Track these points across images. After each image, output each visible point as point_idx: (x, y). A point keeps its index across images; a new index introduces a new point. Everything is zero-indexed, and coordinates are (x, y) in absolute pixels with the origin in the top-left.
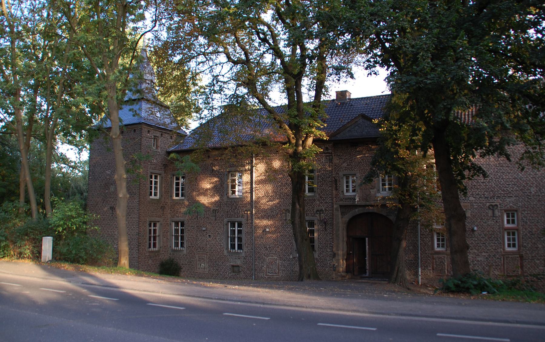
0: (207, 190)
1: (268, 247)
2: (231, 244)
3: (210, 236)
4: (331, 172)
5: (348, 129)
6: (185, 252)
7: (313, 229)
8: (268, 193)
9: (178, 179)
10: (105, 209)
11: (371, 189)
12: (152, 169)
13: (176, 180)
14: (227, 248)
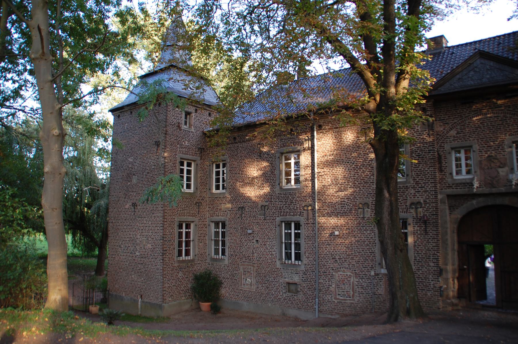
0: (253, 178)
1: (337, 257)
3: (257, 241)
4: (432, 144)
5: (458, 76)
6: (226, 262)
7: (406, 231)
8: (336, 179)
9: (218, 167)
10: (127, 206)
11: (500, 167)
12: (183, 153)
14: (281, 259)
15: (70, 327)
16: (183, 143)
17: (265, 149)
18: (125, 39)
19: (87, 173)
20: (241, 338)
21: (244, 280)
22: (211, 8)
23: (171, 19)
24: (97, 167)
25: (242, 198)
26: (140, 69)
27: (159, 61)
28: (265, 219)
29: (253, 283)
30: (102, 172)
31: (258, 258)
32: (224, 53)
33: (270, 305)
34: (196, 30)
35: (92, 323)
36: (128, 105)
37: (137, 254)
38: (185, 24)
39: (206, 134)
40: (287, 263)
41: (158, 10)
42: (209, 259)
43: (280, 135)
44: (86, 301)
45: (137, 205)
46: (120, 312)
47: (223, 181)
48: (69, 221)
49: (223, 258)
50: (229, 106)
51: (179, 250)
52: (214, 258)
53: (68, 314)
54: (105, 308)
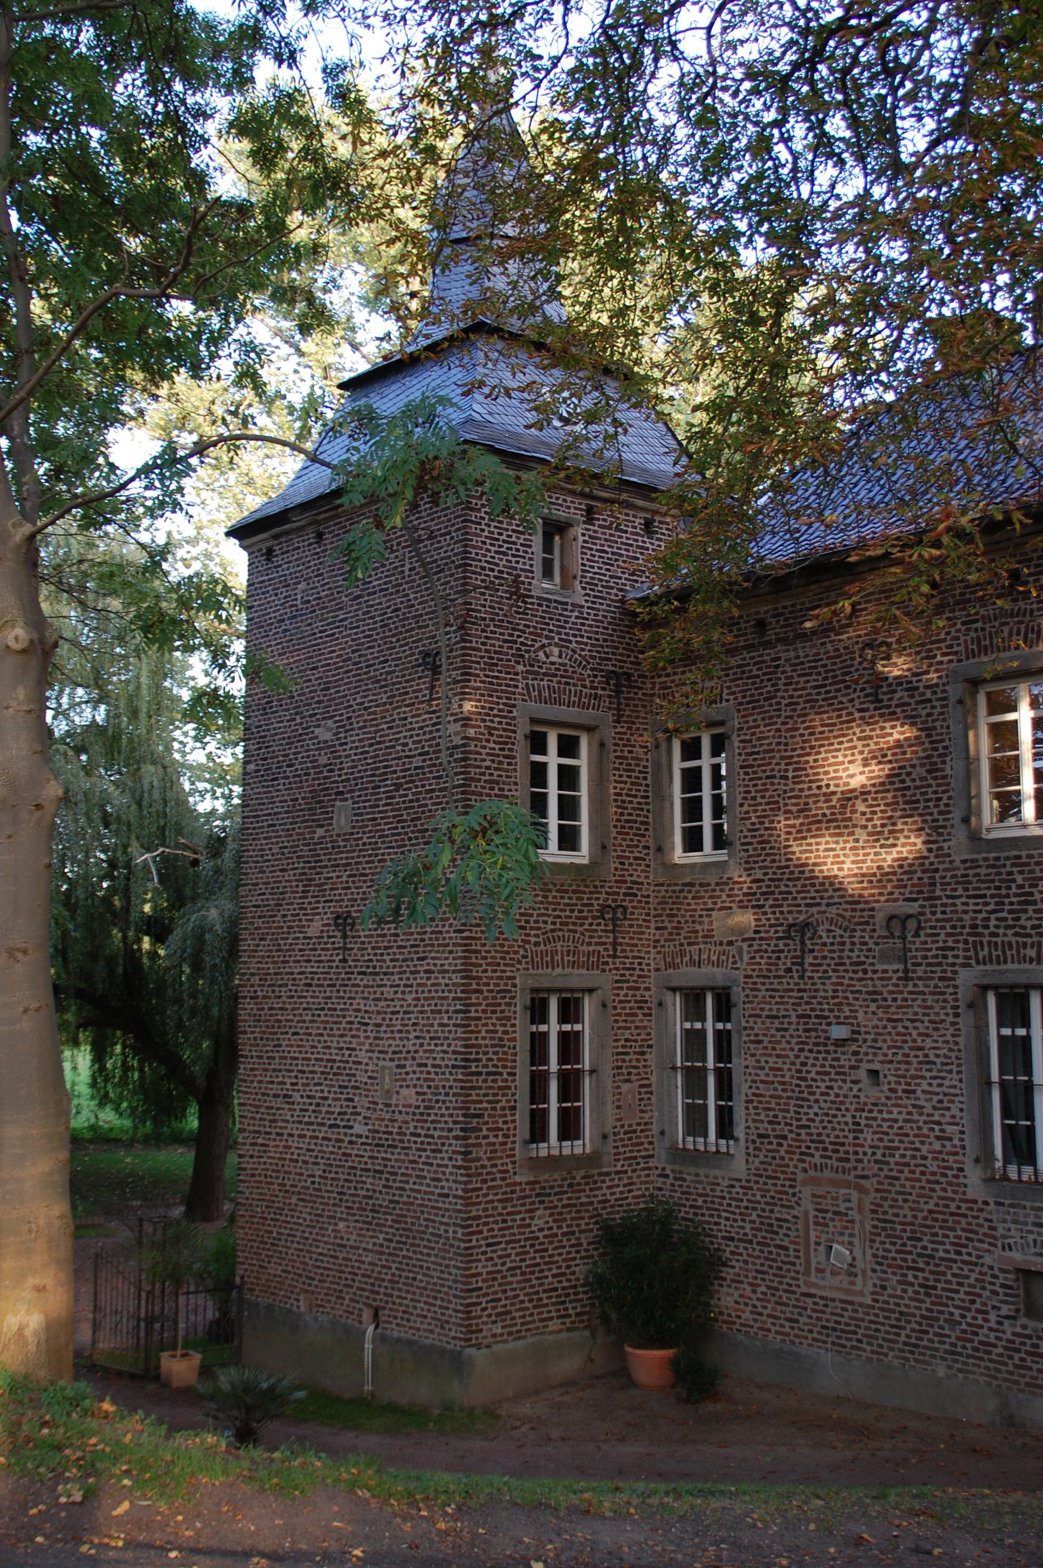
0: (849, 797)
2: (1004, 1127)
3: (874, 1073)
6: (739, 1167)
9: (692, 750)
10: (314, 929)
12: (540, 698)
13: (684, 759)
14: (985, 1157)
15: (79, 1454)
16: (541, 654)
17: (898, 667)
18: (278, 229)
19: (150, 794)
20: (812, 1527)
21: (822, 1249)
22: (632, 57)
23: (464, 126)
24: (190, 767)
25: (799, 883)
26: (346, 348)
27: (424, 313)
28: (906, 978)
29: (859, 1263)
30: (208, 786)
31: (879, 1153)
32: (698, 258)
33: (941, 1372)
34: (575, 167)
35: (169, 1436)
36: (304, 507)
37: (359, 1129)
38: (527, 138)
39: (635, 615)
40: (1014, 1176)
41: (408, 92)
42: (664, 1155)
43: (963, 602)
44: (149, 1332)
45: (353, 925)
46: (285, 1383)
47: (718, 810)
48: (80, 994)
49: (724, 1150)
50: (730, 485)
51: (532, 1110)
52: (684, 1149)
53: (70, 1393)
54: (223, 1365)
